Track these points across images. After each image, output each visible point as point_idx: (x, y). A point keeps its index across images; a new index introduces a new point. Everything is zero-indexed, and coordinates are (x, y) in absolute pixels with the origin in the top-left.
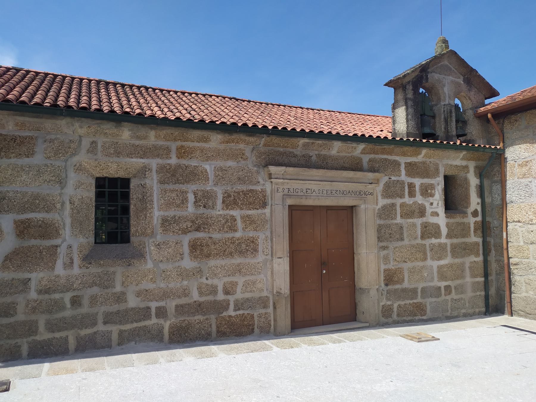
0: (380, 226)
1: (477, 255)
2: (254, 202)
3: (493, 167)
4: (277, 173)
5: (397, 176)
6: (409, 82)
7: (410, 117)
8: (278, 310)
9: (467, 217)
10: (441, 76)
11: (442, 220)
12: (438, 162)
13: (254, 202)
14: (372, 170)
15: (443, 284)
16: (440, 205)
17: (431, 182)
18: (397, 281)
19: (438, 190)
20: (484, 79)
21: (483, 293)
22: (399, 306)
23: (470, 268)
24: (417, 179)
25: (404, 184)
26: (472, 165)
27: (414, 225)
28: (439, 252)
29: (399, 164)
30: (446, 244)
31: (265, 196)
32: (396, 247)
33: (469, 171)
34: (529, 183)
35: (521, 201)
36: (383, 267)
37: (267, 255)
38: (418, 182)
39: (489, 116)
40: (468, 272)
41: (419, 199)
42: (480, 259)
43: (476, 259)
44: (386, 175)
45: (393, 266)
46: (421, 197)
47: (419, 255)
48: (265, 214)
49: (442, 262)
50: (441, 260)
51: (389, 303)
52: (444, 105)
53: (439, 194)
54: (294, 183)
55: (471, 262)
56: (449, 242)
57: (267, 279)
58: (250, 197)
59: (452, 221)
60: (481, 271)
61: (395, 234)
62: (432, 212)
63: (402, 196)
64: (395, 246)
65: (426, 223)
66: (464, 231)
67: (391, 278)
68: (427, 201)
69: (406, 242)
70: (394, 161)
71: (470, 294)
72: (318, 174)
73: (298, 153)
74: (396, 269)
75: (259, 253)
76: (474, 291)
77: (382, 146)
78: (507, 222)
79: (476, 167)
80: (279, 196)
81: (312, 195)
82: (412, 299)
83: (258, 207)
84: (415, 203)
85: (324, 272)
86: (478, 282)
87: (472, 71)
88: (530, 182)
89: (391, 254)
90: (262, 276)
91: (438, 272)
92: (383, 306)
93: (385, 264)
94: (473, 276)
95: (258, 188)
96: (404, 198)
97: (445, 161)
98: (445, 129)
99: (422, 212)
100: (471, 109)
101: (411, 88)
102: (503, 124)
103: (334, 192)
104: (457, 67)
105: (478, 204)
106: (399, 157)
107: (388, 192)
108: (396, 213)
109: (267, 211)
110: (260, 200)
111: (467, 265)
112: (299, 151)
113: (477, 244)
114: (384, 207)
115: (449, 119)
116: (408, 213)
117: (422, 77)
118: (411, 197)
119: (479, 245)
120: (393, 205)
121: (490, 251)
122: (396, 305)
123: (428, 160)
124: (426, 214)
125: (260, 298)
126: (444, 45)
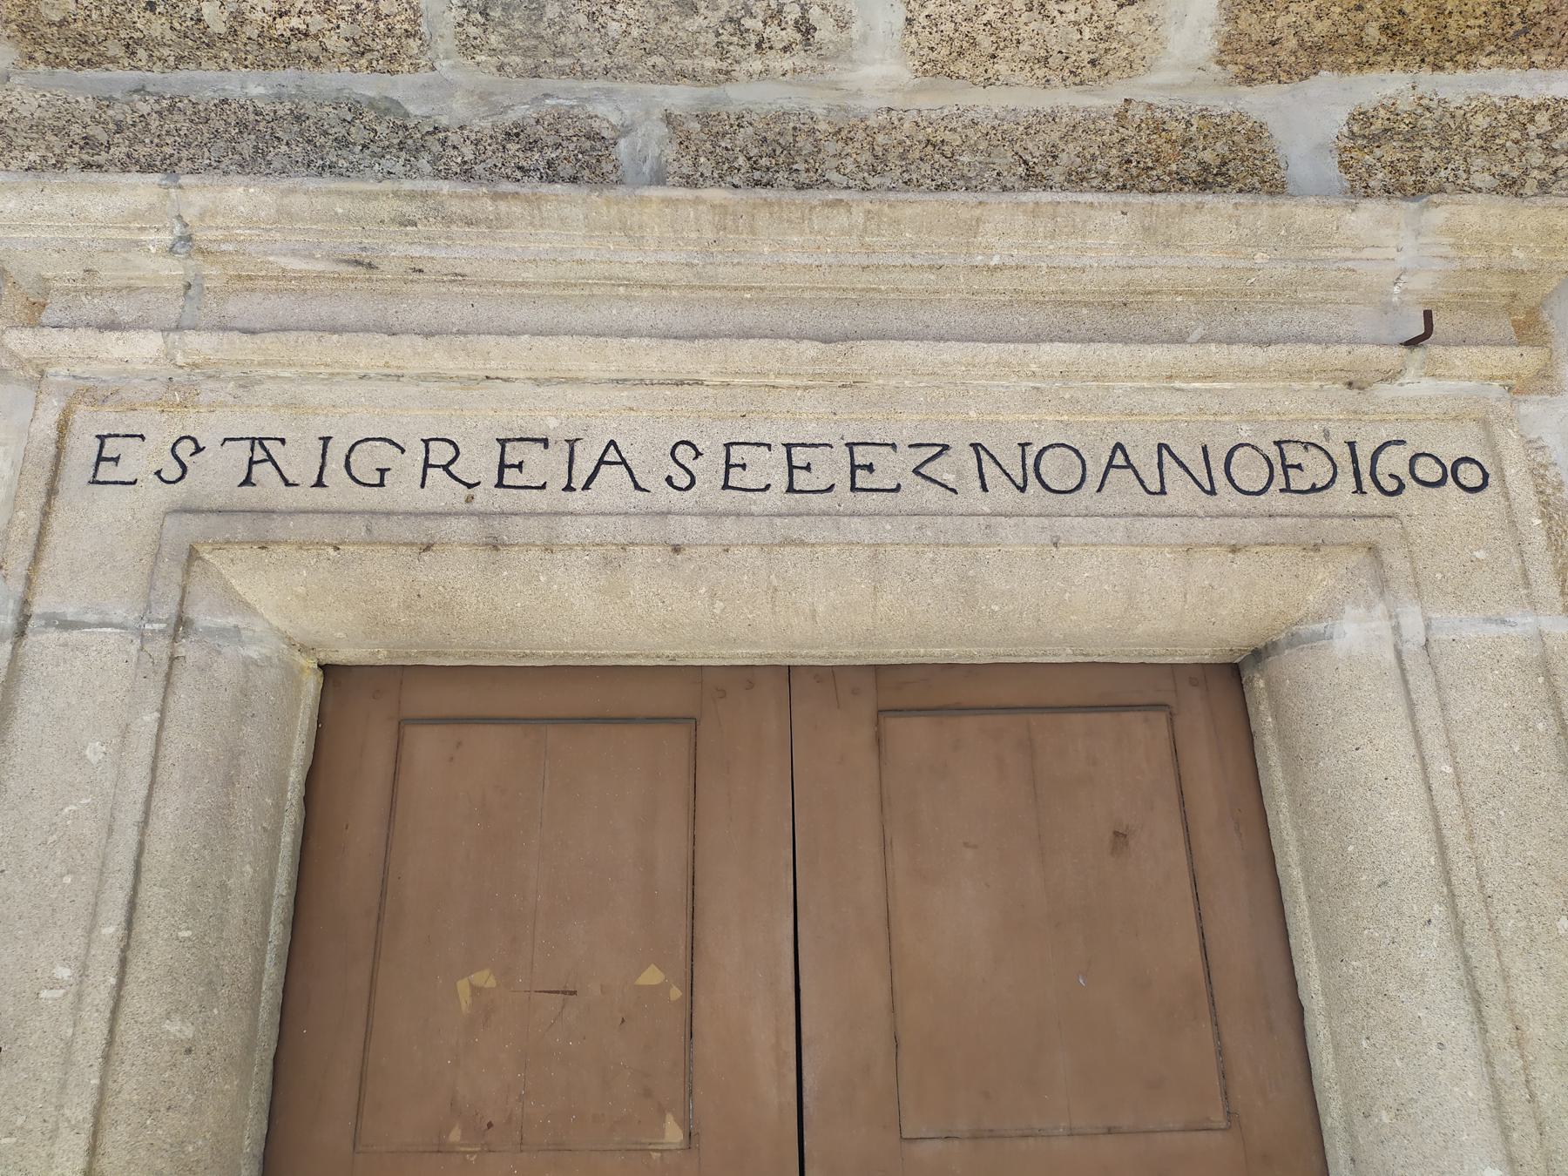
81: (578, 500)
103: (892, 467)
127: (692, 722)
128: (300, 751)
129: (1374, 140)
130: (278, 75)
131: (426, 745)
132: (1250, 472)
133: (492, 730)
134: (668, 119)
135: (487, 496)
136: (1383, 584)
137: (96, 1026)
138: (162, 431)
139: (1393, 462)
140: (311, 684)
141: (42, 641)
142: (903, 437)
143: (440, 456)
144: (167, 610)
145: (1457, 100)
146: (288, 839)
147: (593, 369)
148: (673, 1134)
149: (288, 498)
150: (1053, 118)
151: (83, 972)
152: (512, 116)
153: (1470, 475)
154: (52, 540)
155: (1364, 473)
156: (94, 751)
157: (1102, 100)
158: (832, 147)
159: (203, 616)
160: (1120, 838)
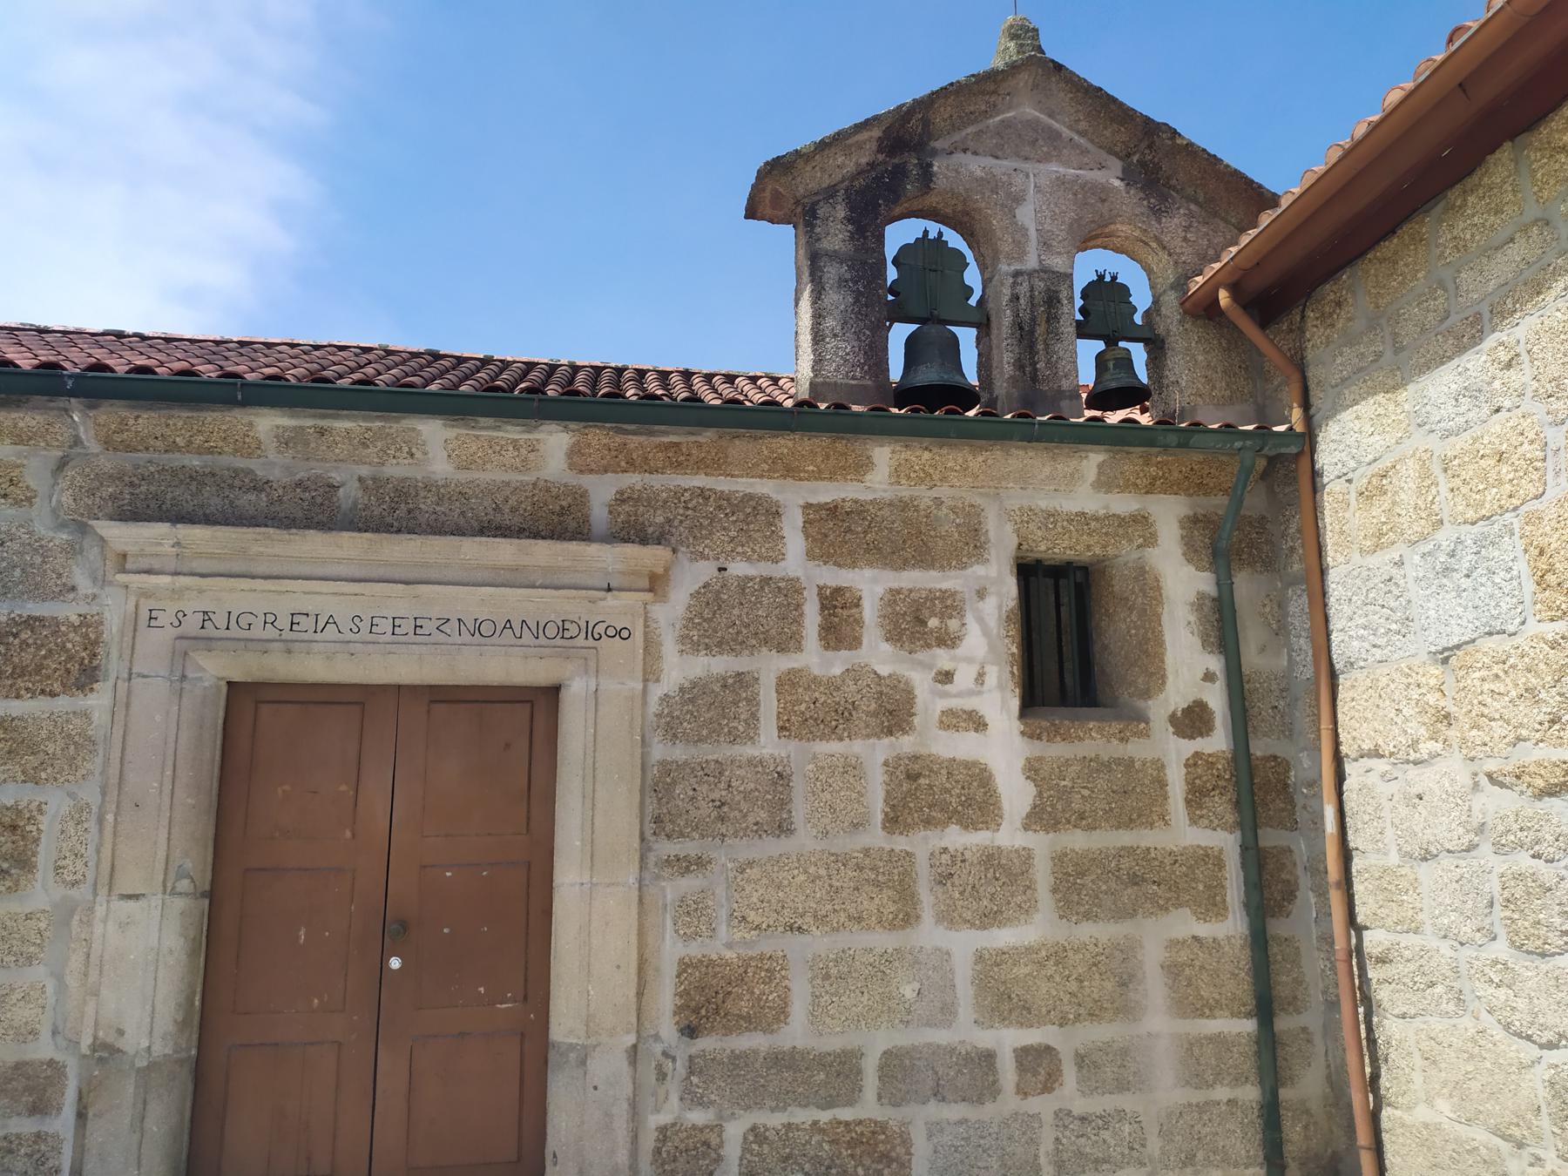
0: (666, 767)
1: (1212, 906)
2: (39, 669)
3: (1264, 513)
4: (149, 550)
5: (761, 558)
6: (830, 193)
7: (830, 323)
8: (91, 1125)
9: (1145, 734)
10: (1002, 166)
11: (1002, 746)
12: (978, 501)
13: (39, 669)
14: (631, 532)
15: (1007, 1040)
16: (992, 677)
17: (944, 586)
18: (748, 1018)
19: (981, 620)
20: (1214, 160)
21: (1250, 1094)
22: (757, 1134)
23: (1173, 970)
24: (868, 573)
25: (799, 591)
26: (1168, 514)
27: (852, 768)
28: (995, 886)
29: (774, 513)
30: (1027, 856)
31: (96, 643)
32: (750, 864)
33: (1154, 536)
34: (1394, 571)
35: (1378, 654)
36: (671, 950)
37: (74, 884)
38: (871, 585)
39: (1224, 297)
40: (1154, 989)
41: (878, 654)
42: (1232, 927)
43: (1204, 930)
44: (703, 556)
45: (729, 946)
46: (886, 647)
47: (885, 901)
48: (86, 715)
49: (1004, 937)
50: (1001, 925)
51: (698, 1117)
52: (1017, 274)
53: (986, 632)
54: (232, 590)
55: (1174, 944)
56: (1040, 844)
57: (62, 986)
58: (25, 645)
59: (1057, 750)
60: (1241, 987)
61: (744, 806)
62: (949, 713)
63: (788, 642)
64: (743, 856)
65: (915, 758)
66: (1135, 797)
67: (707, 1003)
68: (921, 663)
69: (804, 839)
70: (750, 497)
71: (1170, 1090)
72: (339, 553)
73: (276, 474)
74: (746, 963)
75: (39, 876)
76: (1196, 1077)
77: (651, 433)
78: (1338, 760)
79: (1193, 523)
80: (156, 642)
81: (318, 636)
82: (829, 1104)
83: (57, 687)
84: (852, 673)
85: (395, 963)
86: (1218, 1040)
87: (1151, 130)
88: (1400, 564)
89: (720, 891)
90: (38, 973)
91: (983, 982)
92: (663, 1130)
93: (687, 938)
94: (1189, 1004)
95: (68, 611)
96: (799, 649)
97: (1016, 499)
98: (1019, 365)
99: (894, 712)
100: (1172, 288)
101: (841, 212)
102: (1302, 331)
103: (429, 627)
104: (1083, 125)
105: (1209, 677)
106: (771, 483)
107: (714, 623)
108: (754, 716)
109: (98, 702)
110: (71, 658)
111: (1152, 956)
112: (275, 465)
113: (1211, 859)
114: (693, 693)
115: (1040, 330)
116: (818, 713)
117: (900, 173)
118: (837, 649)
119: (1220, 864)
120: (742, 682)
121: (1290, 894)
122: (735, 1131)
123: (924, 495)
124: (916, 720)
125: (18, 1066)
126: (1012, 44)
127: (363, 704)
128: (221, 714)
129: (623, 501)
130: (205, 457)
131: (265, 710)
132: (551, 631)
133: (289, 706)
134: (360, 479)
135: (287, 635)
136: (586, 672)
137: (167, 800)
138: (172, 607)
139: (600, 629)
140: (224, 690)
141: (136, 681)
142: (434, 617)
143: (270, 620)
144: (178, 673)
145: (657, 486)
146: (219, 742)
147: (324, 590)
148: (348, 834)
149: (217, 634)
150: (508, 484)
151: (161, 785)
152: (298, 477)
153: (625, 634)
154: (137, 646)
155: (589, 632)
156: (158, 718)
157: (529, 478)
158: (422, 494)
159: (190, 675)
160: (508, 746)
